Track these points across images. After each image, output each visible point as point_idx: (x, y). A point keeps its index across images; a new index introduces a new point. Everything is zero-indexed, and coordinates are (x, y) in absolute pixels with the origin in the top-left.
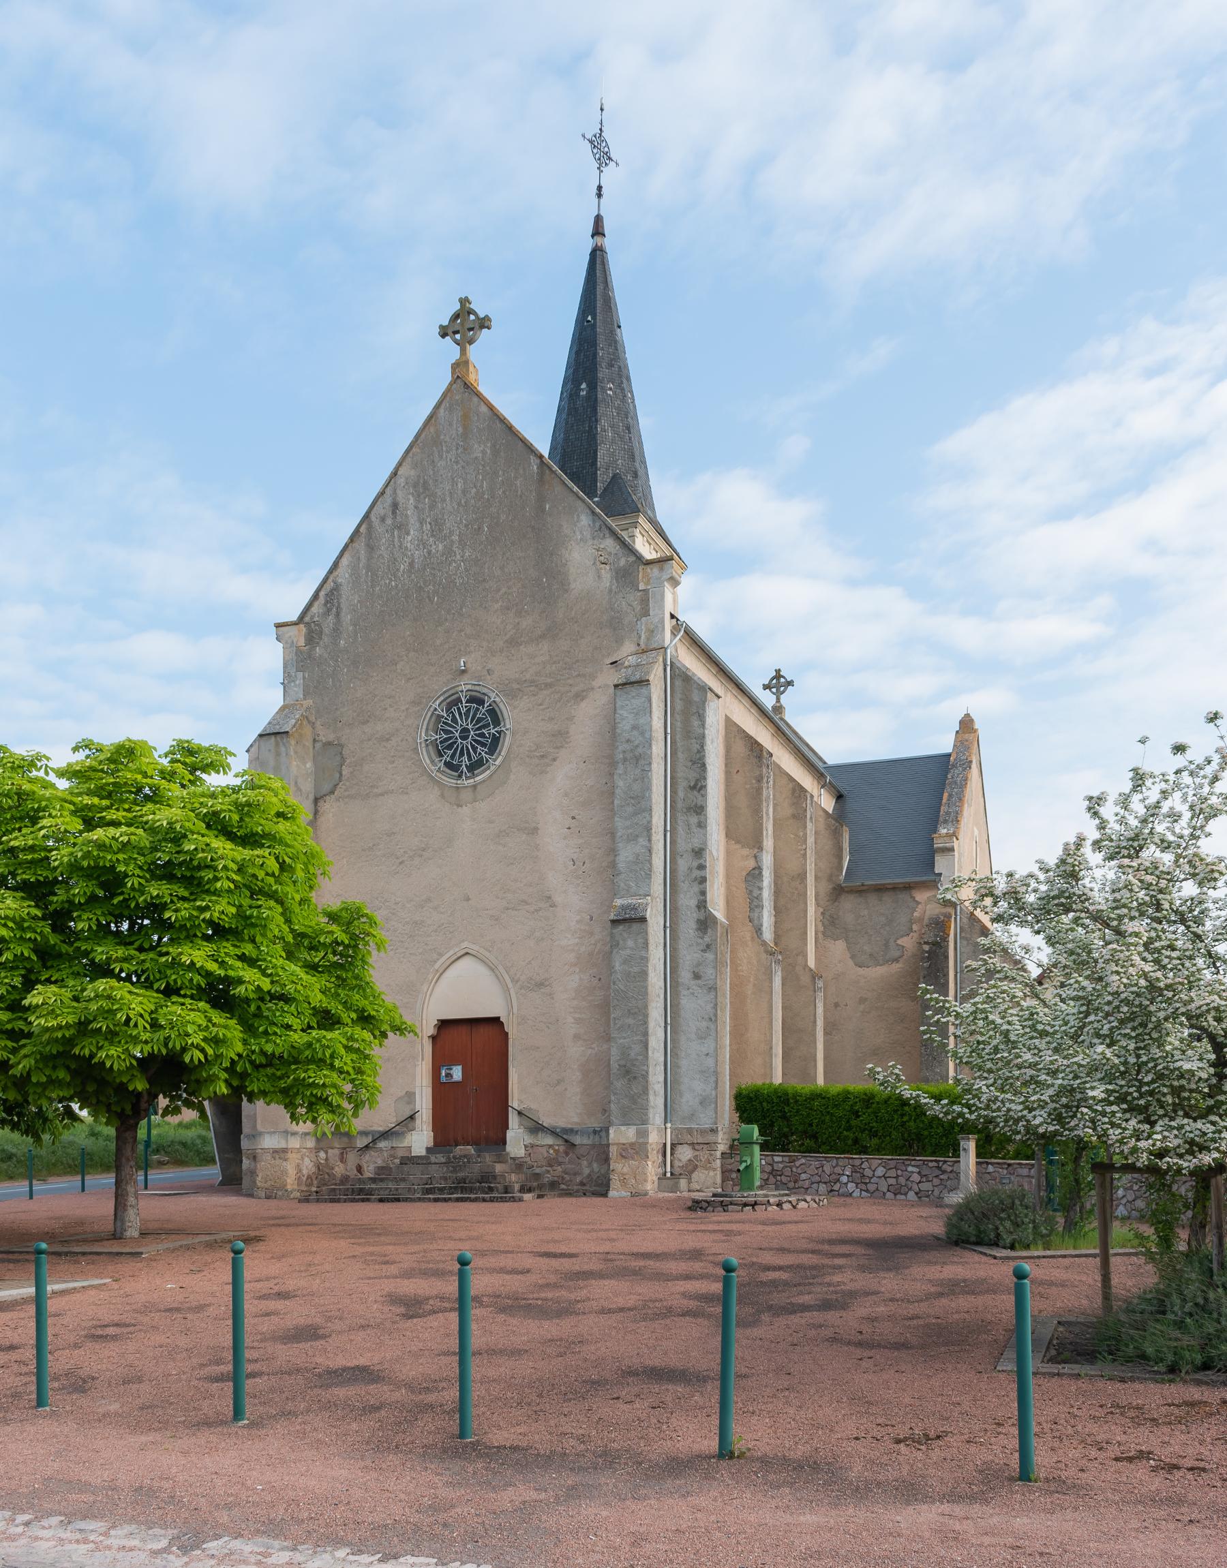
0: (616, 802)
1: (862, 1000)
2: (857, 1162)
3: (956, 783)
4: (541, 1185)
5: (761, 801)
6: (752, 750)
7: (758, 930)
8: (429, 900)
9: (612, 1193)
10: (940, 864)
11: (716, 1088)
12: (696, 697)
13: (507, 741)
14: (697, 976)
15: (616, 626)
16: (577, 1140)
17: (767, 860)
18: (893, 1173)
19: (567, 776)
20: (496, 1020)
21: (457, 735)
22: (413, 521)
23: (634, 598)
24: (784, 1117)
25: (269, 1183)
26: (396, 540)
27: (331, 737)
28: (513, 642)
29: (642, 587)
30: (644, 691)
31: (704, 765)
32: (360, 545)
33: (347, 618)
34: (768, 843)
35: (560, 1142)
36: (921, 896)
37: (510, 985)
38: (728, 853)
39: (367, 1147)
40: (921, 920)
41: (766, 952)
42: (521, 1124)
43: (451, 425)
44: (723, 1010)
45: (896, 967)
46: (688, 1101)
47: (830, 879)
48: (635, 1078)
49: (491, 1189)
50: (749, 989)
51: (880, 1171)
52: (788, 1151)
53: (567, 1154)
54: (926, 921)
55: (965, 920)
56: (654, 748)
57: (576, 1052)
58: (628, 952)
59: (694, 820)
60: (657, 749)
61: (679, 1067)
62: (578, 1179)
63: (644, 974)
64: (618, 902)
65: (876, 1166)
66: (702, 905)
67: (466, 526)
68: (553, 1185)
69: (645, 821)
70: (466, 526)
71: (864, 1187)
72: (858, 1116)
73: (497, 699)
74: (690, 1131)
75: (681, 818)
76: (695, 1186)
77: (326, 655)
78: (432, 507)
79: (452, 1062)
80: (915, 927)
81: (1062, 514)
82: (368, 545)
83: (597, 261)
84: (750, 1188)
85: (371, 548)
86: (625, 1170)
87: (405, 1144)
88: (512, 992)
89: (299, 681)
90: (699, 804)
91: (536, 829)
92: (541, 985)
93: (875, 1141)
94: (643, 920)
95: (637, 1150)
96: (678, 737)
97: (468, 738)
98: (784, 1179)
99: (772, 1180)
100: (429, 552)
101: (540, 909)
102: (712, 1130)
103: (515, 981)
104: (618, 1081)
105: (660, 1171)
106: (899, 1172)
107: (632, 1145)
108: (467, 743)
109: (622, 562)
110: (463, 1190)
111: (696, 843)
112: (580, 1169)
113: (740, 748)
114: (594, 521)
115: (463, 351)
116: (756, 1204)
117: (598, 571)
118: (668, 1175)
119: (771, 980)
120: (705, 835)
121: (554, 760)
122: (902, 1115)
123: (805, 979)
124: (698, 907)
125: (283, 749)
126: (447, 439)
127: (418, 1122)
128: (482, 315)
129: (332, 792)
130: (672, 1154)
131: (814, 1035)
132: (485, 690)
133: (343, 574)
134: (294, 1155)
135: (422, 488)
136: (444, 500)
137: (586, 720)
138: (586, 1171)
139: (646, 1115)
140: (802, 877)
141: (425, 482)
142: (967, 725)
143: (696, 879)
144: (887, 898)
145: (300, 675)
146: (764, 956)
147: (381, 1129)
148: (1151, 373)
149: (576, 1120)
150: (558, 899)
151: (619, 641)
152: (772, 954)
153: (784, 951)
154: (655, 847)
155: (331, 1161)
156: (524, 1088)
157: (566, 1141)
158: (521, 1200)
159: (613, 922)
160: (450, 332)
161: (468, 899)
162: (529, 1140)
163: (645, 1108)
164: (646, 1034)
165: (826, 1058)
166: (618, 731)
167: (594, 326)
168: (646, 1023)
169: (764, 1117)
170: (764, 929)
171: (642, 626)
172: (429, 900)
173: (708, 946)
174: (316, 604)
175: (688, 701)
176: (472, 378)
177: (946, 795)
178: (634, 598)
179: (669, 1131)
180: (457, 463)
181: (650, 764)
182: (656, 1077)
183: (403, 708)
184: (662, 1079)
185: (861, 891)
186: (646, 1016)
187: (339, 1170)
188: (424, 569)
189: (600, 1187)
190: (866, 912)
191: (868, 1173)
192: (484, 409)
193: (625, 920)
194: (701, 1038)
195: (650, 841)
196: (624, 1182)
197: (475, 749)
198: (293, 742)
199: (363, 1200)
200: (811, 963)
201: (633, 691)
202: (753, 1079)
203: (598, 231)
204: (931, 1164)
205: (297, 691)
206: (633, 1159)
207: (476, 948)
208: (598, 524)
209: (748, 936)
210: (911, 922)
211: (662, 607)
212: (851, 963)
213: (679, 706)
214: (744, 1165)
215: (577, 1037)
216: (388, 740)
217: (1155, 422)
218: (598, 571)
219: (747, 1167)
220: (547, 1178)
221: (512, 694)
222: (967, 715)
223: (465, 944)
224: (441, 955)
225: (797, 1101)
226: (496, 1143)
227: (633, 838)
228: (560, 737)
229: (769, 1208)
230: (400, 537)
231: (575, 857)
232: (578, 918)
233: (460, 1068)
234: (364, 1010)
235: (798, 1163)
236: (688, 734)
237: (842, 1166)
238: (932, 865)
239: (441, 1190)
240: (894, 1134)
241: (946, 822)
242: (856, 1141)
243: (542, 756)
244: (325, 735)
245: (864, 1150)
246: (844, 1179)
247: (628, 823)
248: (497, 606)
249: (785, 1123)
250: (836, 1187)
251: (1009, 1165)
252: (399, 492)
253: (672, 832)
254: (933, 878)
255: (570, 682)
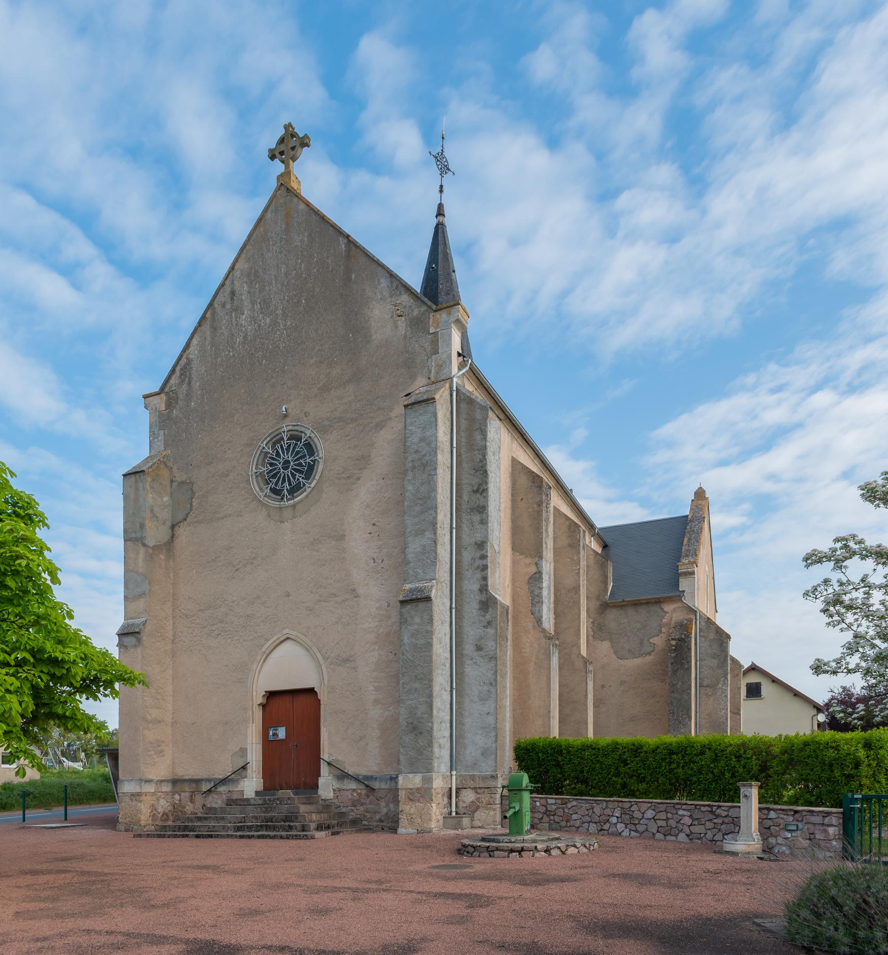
0: (406, 503)
1: (623, 683)
2: (627, 805)
3: (693, 531)
4: (337, 822)
5: (541, 520)
6: (533, 482)
7: (539, 621)
8: (258, 597)
9: (401, 830)
10: (684, 584)
11: (496, 741)
12: (478, 415)
13: (320, 468)
14: (479, 648)
15: (409, 365)
16: (376, 785)
17: (548, 567)
18: (663, 816)
19: (368, 490)
20: (311, 691)
21: (280, 466)
22: (247, 303)
23: (426, 341)
24: (558, 765)
25: (128, 819)
26: (234, 320)
27: (184, 478)
28: (325, 389)
29: (432, 330)
30: (430, 408)
31: (486, 472)
32: (206, 328)
33: (196, 385)
34: (548, 554)
35: (362, 787)
36: (669, 607)
37: (322, 662)
38: (514, 563)
39: (210, 791)
40: (668, 624)
41: (545, 637)
42: (330, 773)
43: (276, 223)
44: (504, 676)
45: (649, 659)
46: (471, 752)
47: (598, 599)
48: (421, 733)
49: (290, 828)
50: (531, 667)
51: (650, 814)
52: (561, 793)
53: (368, 796)
54: (673, 624)
55: (703, 624)
56: (439, 456)
57: (375, 713)
58: (415, 627)
59: (477, 518)
60: (443, 458)
61: (463, 724)
62: (378, 817)
63: (429, 645)
64: (408, 586)
65: (646, 809)
66: (484, 588)
67: (288, 301)
68: (355, 822)
69: (431, 518)
70: (288, 301)
71: (633, 827)
72: (627, 764)
73: (312, 435)
74: (473, 777)
75: (465, 517)
76: (477, 823)
77: (181, 415)
78: (261, 291)
79: (277, 725)
80: (663, 630)
81: (723, 463)
82: (212, 327)
83: (439, 231)
84: (519, 833)
85: (214, 329)
86: (412, 811)
87: (239, 788)
88: (323, 666)
89: (161, 438)
90: (481, 504)
91: (344, 536)
92: (346, 660)
93: (643, 786)
94: (428, 599)
95: (423, 794)
96: (463, 450)
97: (289, 469)
98: (557, 819)
99: (546, 819)
100: (259, 326)
101: (347, 600)
102: (492, 777)
103: (325, 658)
104: (411, 734)
105: (446, 811)
106: (669, 815)
107: (418, 789)
108: (288, 472)
109: (416, 313)
110: (268, 828)
111: (478, 537)
112: (374, 811)
113: (523, 481)
114: (391, 282)
115: (287, 166)
116: (522, 850)
117: (395, 322)
118: (454, 814)
119: (549, 659)
120: (487, 530)
121: (358, 479)
122: (670, 763)
123: (579, 664)
124: (480, 590)
125: (141, 485)
126: (273, 235)
127: (249, 771)
128: (301, 135)
129: (185, 520)
130: (457, 797)
131: (586, 705)
132: (302, 429)
133: (194, 351)
134: (148, 798)
135: (253, 276)
136: (270, 284)
137: (384, 446)
138: (384, 811)
139: (431, 764)
140: (577, 589)
141: (256, 271)
142: (700, 494)
143: (478, 567)
144: (642, 610)
145: (162, 432)
146: (543, 640)
147: (221, 777)
148: (774, 391)
149: (375, 769)
150: (361, 591)
151: (413, 378)
152: (550, 638)
153: (561, 638)
154: (440, 541)
155: (183, 802)
156: (332, 744)
157: (367, 786)
158: (313, 838)
159: (402, 602)
160: (277, 155)
161: (289, 595)
162: (336, 785)
163: (429, 759)
164: (430, 696)
165: (595, 724)
166: (408, 444)
167: (436, 271)
168: (430, 686)
169: (540, 766)
170: (544, 619)
171: (433, 363)
172: (258, 597)
173: (489, 623)
174: (173, 377)
175: (471, 420)
176: (294, 185)
177: (686, 539)
178: (426, 341)
179: (454, 778)
180: (281, 252)
181: (436, 469)
182: (442, 733)
183: (239, 450)
184: (447, 734)
185: (622, 606)
186: (431, 680)
187: (189, 808)
188: (255, 340)
189: (391, 824)
190: (625, 621)
191: (637, 814)
192: (302, 206)
193: (412, 601)
194: (483, 700)
195: (435, 533)
196: (411, 821)
197: (294, 476)
198: (149, 479)
199: (183, 836)
200: (584, 652)
201: (421, 408)
202: (534, 733)
203: (440, 212)
204: (703, 809)
205: (160, 445)
206: (419, 801)
207: (295, 633)
208: (395, 285)
209: (530, 626)
210: (661, 626)
211: (449, 345)
212: (614, 656)
213: (464, 424)
214: (511, 811)
215: (376, 702)
216: (227, 476)
217: (776, 415)
218: (395, 322)
219: (515, 813)
220: (352, 816)
221: (324, 430)
222: (701, 488)
223: (286, 631)
224: (267, 640)
225: (569, 752)
226: (313, 788)
227: (420, 533)
228: (363, 461)
229: (537, 855)
230: (236, 317)
231: (375, 556)
232: (378, 605)
233: (284, 729)
234: (41, 650)
235: (569, 805)
236: (471, 446)
237: (611, 807)
238: (677, 585)
239: (250, 828)
240: (662, 780)
241: (687, 556)
242: (624, 786)
243: (349, 477)
244: (180, 476)
245: (632, 794)
246: (614, 820)
247: (416, 520)
248: (312, 361)
249: (550, 768)
250: (606, 827)
251: (796, 812)
252: (236, 283)
253: (458, 528)
254: (678, 594)
255: (372, 415)
